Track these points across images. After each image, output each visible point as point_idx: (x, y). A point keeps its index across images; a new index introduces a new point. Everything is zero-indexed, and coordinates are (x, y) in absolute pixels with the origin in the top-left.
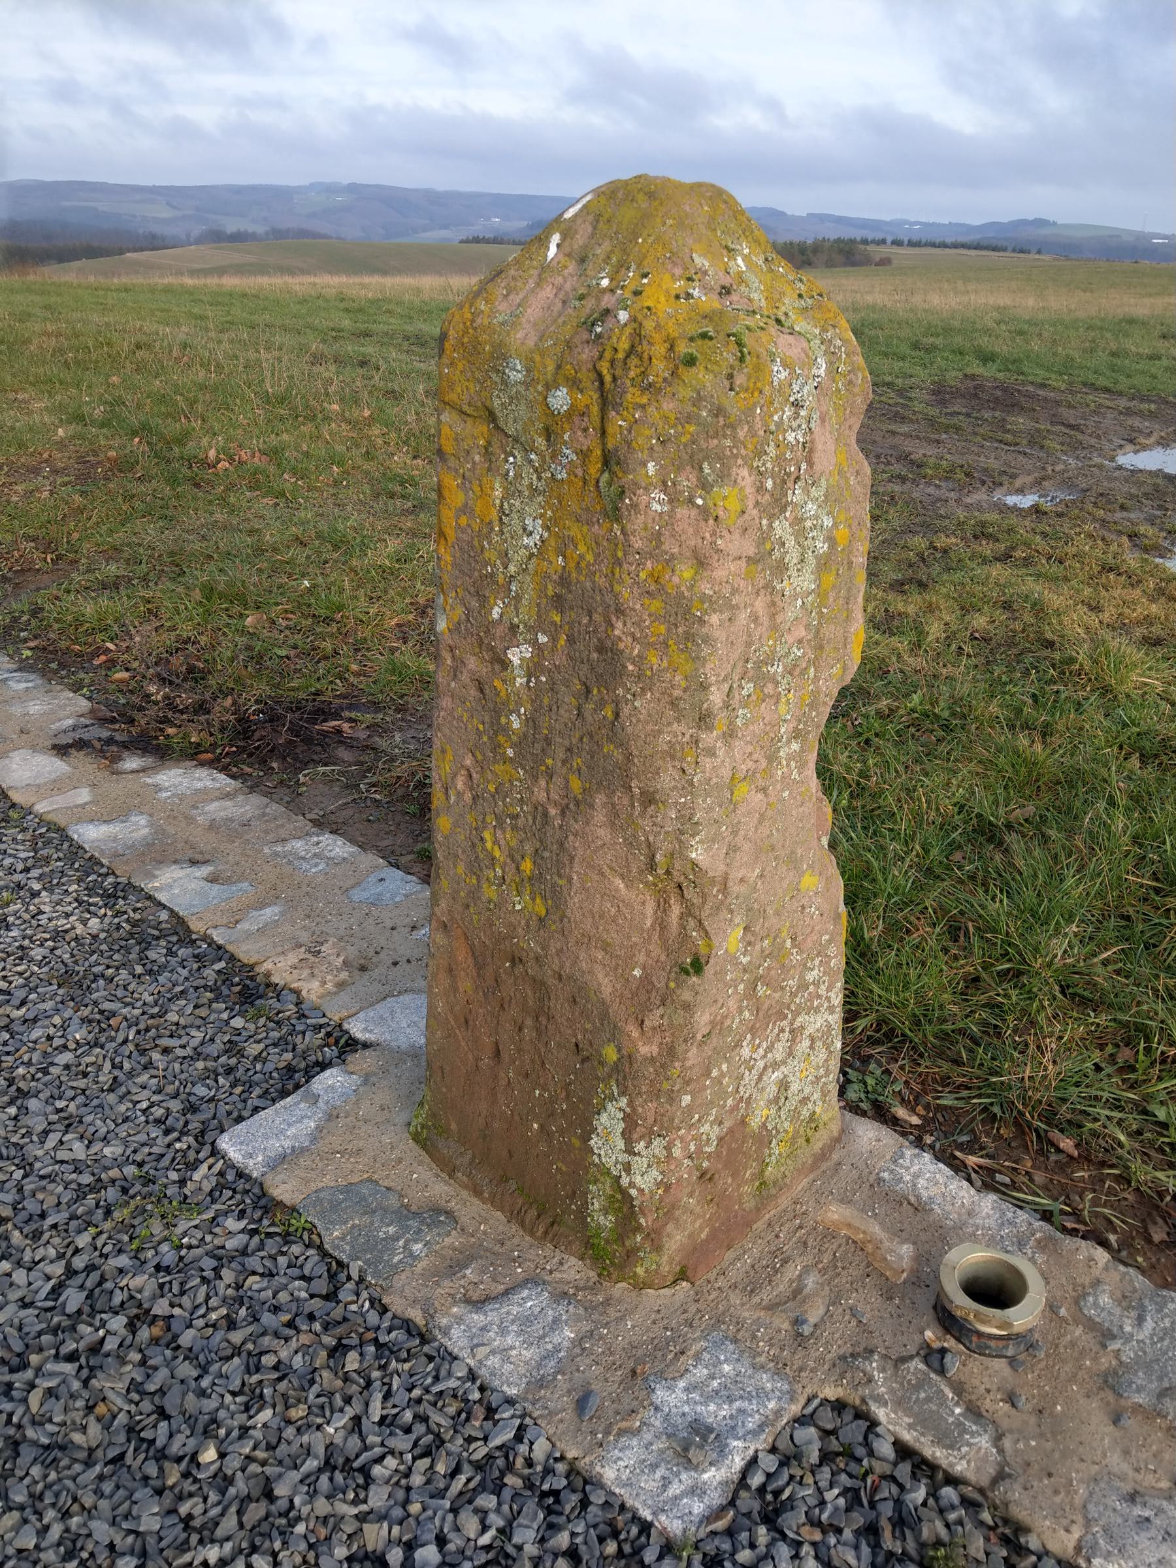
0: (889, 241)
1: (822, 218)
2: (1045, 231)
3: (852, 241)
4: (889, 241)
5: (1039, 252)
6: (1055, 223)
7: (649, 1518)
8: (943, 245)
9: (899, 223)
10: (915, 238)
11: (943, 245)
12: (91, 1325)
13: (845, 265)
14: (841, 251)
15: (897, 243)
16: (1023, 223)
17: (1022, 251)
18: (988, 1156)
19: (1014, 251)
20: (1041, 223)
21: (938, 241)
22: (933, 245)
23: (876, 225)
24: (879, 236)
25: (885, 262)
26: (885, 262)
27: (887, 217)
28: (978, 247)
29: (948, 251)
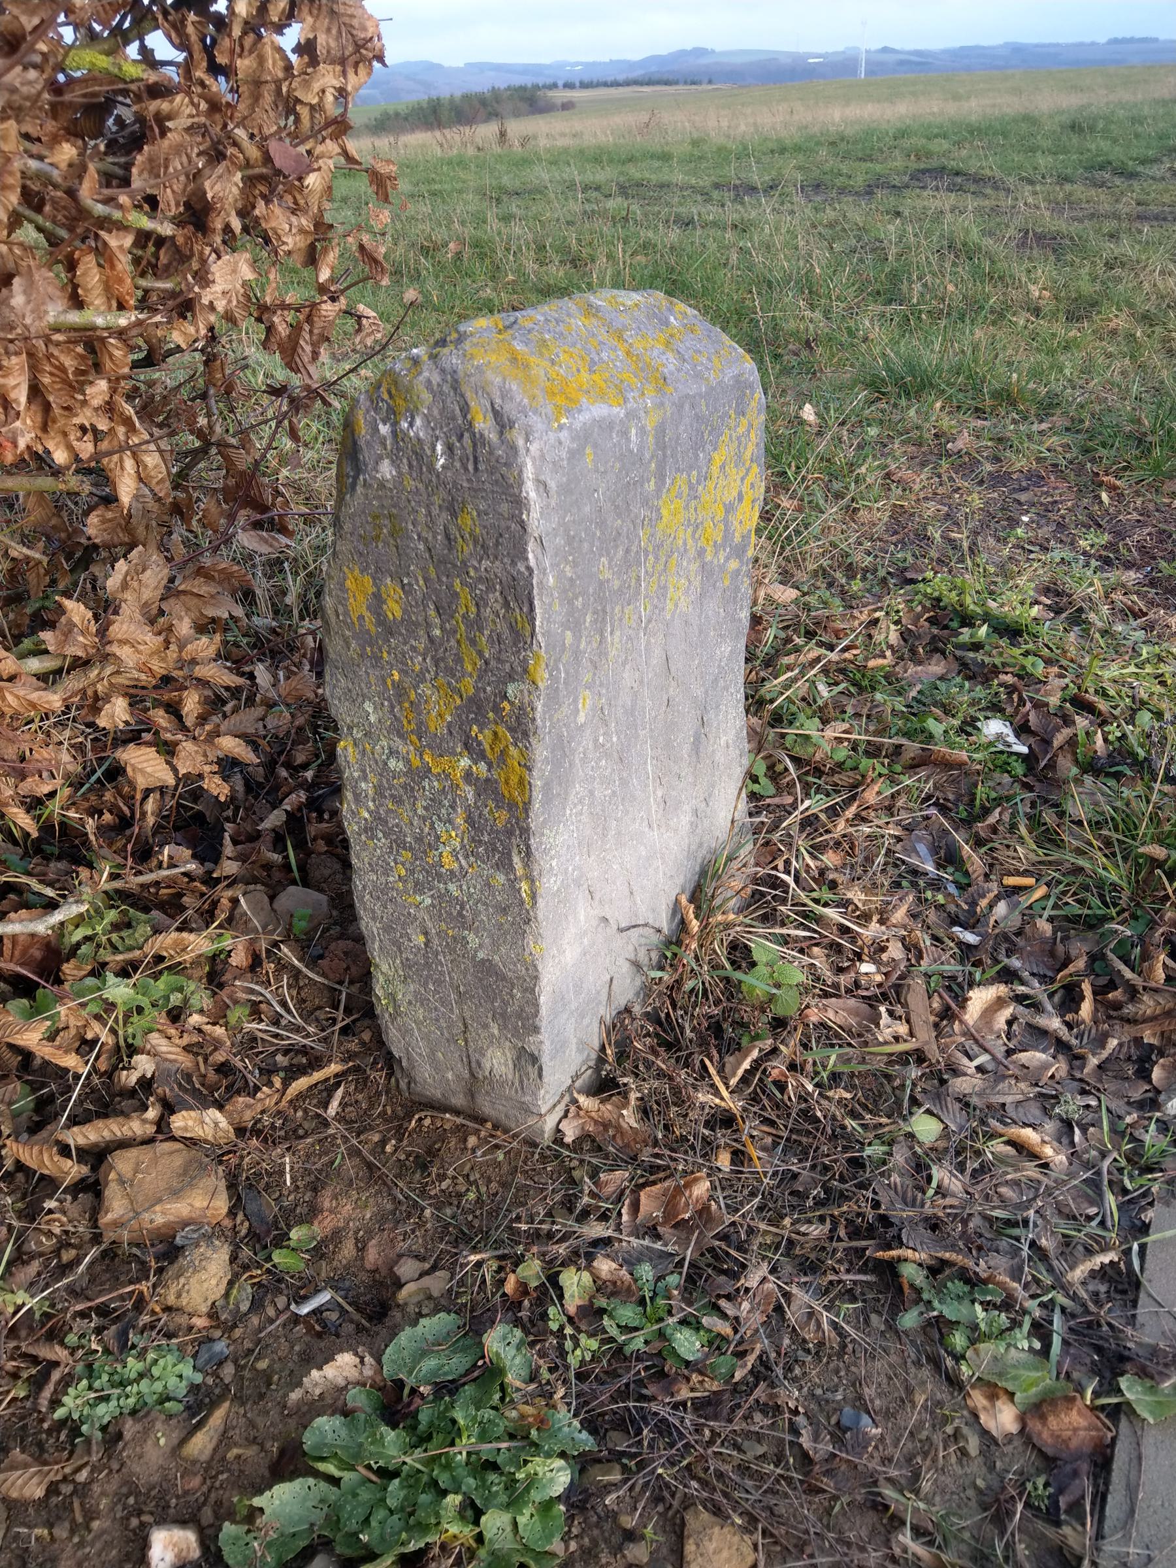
0: (560, 83)
1: (481, 67)
2: (704, 61)
3: (536, 87)
4: (560, 83)
5: (710, 82)
6: (713, 51)
7: (1085, 958)
8: (616, 84)
9: (560, 66)
10: (586, 79)
11: (616, 84)
12: (68, 1381)
13: (533, 113)
14: (522, 99)
15: (569, 86)
16: (682, 53)
17: (693, 83)
18: (862, 1125)
19: (686, 83)
20: (699, 52)
21: (610, 79)
22: (606, 84)
23: (537, 69)
24: (549, 81)
25: (567, 106)
26: (567, 106)
27: (546, 60)
28: (650, 83)
29: (621, 89)
